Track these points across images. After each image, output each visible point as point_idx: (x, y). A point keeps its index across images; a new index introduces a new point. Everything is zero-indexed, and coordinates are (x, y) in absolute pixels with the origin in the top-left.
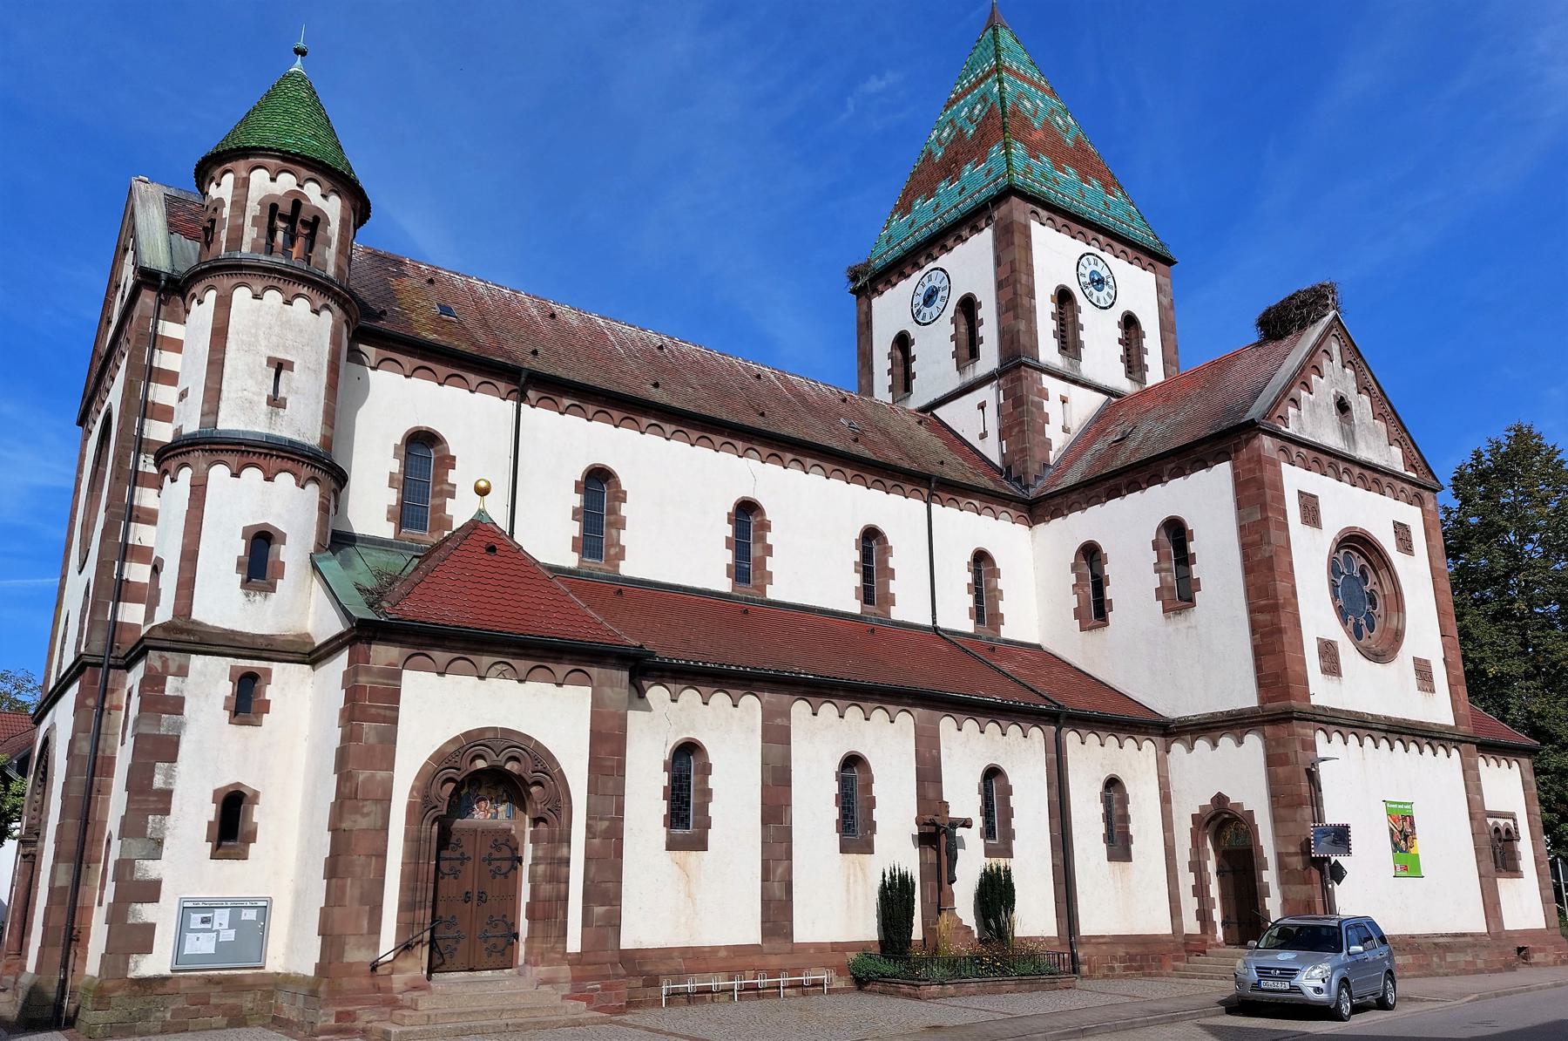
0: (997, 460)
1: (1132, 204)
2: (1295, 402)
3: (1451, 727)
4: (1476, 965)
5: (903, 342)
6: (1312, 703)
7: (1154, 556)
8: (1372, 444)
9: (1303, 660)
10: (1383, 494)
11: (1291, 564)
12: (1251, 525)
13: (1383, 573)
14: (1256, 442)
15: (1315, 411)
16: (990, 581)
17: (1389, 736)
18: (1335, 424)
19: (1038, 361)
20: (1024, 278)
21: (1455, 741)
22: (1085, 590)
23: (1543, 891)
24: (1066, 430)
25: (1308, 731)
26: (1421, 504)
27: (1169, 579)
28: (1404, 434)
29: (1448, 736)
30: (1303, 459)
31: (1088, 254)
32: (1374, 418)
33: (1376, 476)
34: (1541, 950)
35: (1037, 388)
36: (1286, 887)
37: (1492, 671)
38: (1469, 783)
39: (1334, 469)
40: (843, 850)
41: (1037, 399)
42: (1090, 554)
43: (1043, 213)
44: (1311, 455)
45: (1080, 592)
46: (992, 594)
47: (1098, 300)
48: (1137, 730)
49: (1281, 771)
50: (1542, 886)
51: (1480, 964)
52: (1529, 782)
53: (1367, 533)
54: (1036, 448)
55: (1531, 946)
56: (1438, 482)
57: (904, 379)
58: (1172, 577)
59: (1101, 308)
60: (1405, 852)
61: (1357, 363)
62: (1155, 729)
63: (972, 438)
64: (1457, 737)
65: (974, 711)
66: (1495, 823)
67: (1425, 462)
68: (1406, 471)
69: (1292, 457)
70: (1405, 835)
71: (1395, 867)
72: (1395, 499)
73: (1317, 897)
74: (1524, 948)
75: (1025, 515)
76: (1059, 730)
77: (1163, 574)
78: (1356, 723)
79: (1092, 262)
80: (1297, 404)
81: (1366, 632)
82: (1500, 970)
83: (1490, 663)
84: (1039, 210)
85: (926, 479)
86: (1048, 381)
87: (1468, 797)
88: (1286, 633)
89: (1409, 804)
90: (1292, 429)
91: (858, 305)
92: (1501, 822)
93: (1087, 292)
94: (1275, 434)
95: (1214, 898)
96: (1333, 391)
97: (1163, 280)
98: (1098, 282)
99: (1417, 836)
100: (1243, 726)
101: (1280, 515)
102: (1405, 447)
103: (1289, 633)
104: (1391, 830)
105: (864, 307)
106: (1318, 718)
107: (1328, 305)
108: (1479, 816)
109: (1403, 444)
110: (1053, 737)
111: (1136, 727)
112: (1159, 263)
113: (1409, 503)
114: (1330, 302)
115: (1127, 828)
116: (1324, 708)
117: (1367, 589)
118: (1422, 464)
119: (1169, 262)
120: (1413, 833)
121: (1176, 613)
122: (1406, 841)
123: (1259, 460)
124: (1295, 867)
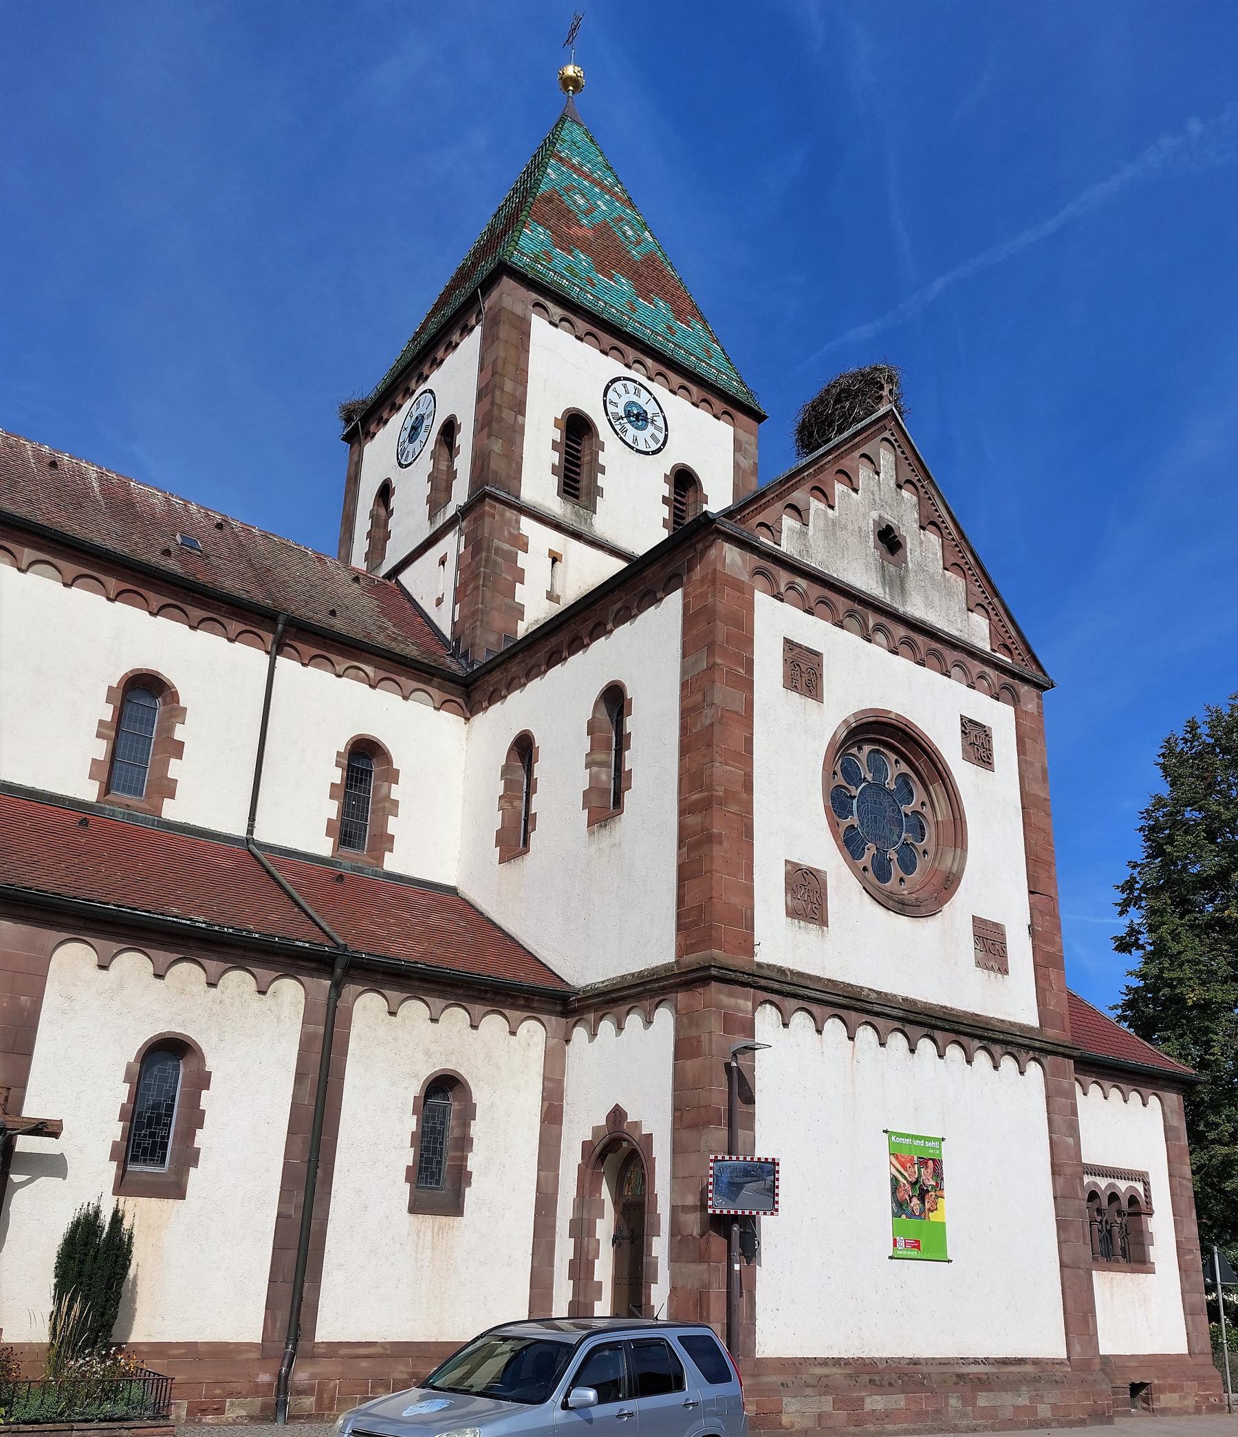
0: (447, 631)
1: (716, 341)
2: (799, 512)
3: (1032, 1029)
4: (1036, 1414)
5: (385, 492)
6: (757, 959)
7: (586, 742)
8: (937, 603)
9: (749, 892)
10: (947, 674)
11: (749, 742)
12: (694, 680)
13: (936, 789)
14: (713, 552)
15: (834, 534)
16: (382, 786)
17: (908, 1028)
18: (871, 560)
19: (518, 497)
20: (509, 386)
21: (1034, 1049)
22: (515, 804)
23: (1186, 1296)
24: (551, 596)
25: (741, 1002)
26: (1015, 701)
27: (604, 777)
28: (995, 600)
29: (1020, 1040)
30: (800, 594)
32: (945, 569)
33: (938, 646)
34: (1173, 1389)
35: (509, 532)
36: (677, 1265)
37: (1191, 998)
38: (1055, 1117)
39: (858, 621)
40: (414, 1208)
41: (506, 547)
42: (524, 748)
43: (557, 311)
44: (817, 591)
45: (506, 806)
46: (381, 805)
48: (510, 1000)
49: (690, 1065)
50: (1187, 1287)
51: (1044, 1411)
52: (1176, 1129)
53: (908, 724)
54: (495, 613)
55: (1156, 1382)
56: (1045, 674)
57: (379, 536)
58: (608, 774)
59: (638, 451)
60: (919, 1217)
61: (923, 486)
62: (546, 1002)
63: (428, 606)
64: (1037, 1044)
65: (139, 938)
66: (1110, 1186)
67: (1029, 650)
68: (994, 651)
69: (809, 602)
70: (921, 1188)
71: (895, 1241)
72: (969, 686)
73: (715, 1285)
74: (1143, 1385)
75: (458, 700)
76: (337, 987)
77: (595, 769)
78: (840, 1000)
79: (632, 391)
80: (801, 516)
81: (895, 869)
82: (1081, 1423)
83: (1190, 986)
84: (549, 305)
85: (270, 619)
86: (528, 526)
87: (1051, 1138)
88: (721, 843)
89: (935, 1139)
90: (787, 546)
91: (351, 454)
92: (1122, 1185)
94: (745, 544)
95: (600, 1283)
96: (875, 515)
97: (744, 436)
98: (639, 418)
99: (946, 1193)
100: (652, 993)
101: (741, 665)
102: (993, 617)
103: (726, 844)
104: (894, 1180)
105: (355, 457)
106: (763, 982)
107: (881, 397)
108: (1068, 1170)
109: (992, 613)
110: (322, 998)
111: (507, 995)
112: (740, 414)
113: (992, 697)
114: (885, 393)
115: (465, 1159)
116: (781, 970)
117: (907, 809)
118: (1021, 647)
119: (759, 417)
120: (939, 1187)
121: (601, 826)
122: (922, 1200)
123: (715, 580)
124: (689, 1232)
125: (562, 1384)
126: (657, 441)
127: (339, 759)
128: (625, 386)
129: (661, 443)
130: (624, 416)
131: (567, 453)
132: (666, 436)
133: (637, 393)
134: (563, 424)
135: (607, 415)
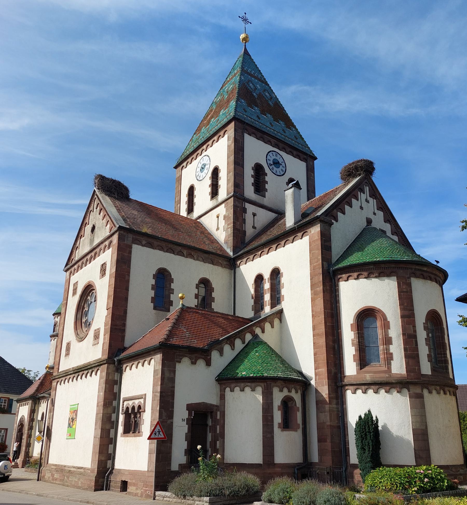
5: (191, 190)
24: (254, 227)
31: (273, 151)
34: (134, 485)
47: (276, 171)
79: (275, 155)
93: (271, 167)
120: (76, 418)
125: (118, 397)
126: (283, 171)
127: (224, 393)
128: (272, 154)
129: (284, 172)
130: (272, 164)
131: (256, 186)
132: (286, 169)
133: (276, 156)
134: (254, 169)
135: (267, 164)
